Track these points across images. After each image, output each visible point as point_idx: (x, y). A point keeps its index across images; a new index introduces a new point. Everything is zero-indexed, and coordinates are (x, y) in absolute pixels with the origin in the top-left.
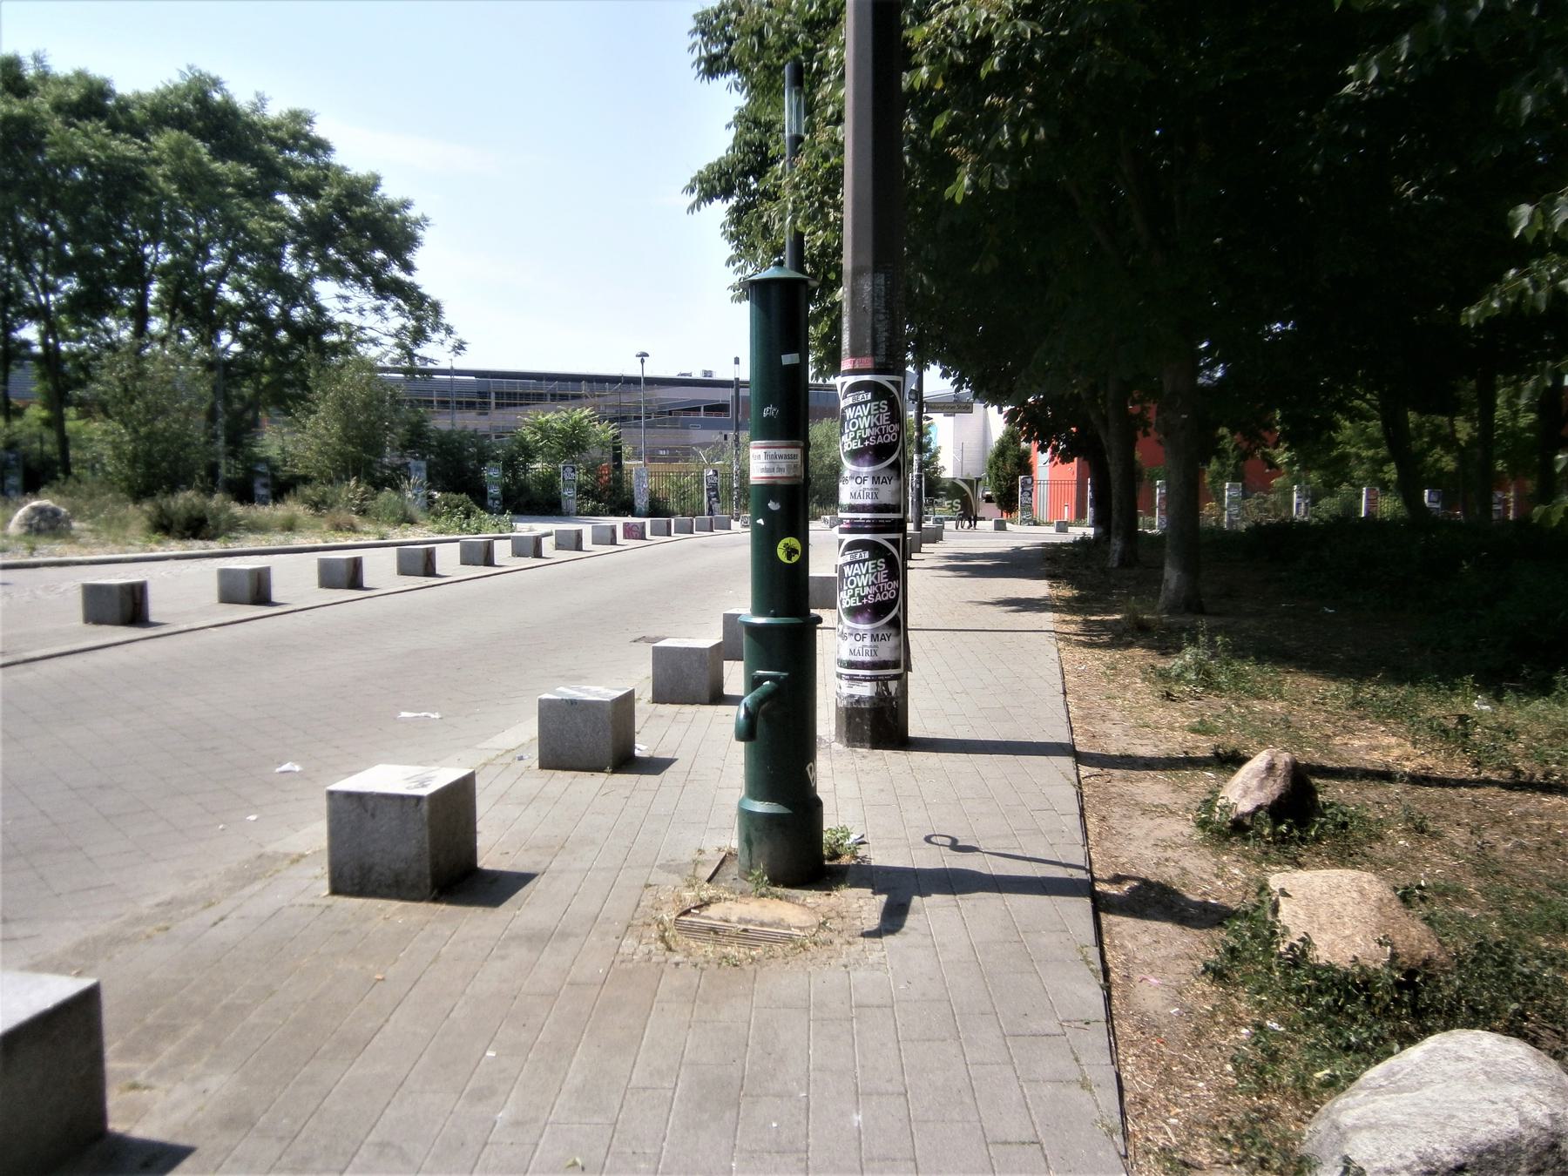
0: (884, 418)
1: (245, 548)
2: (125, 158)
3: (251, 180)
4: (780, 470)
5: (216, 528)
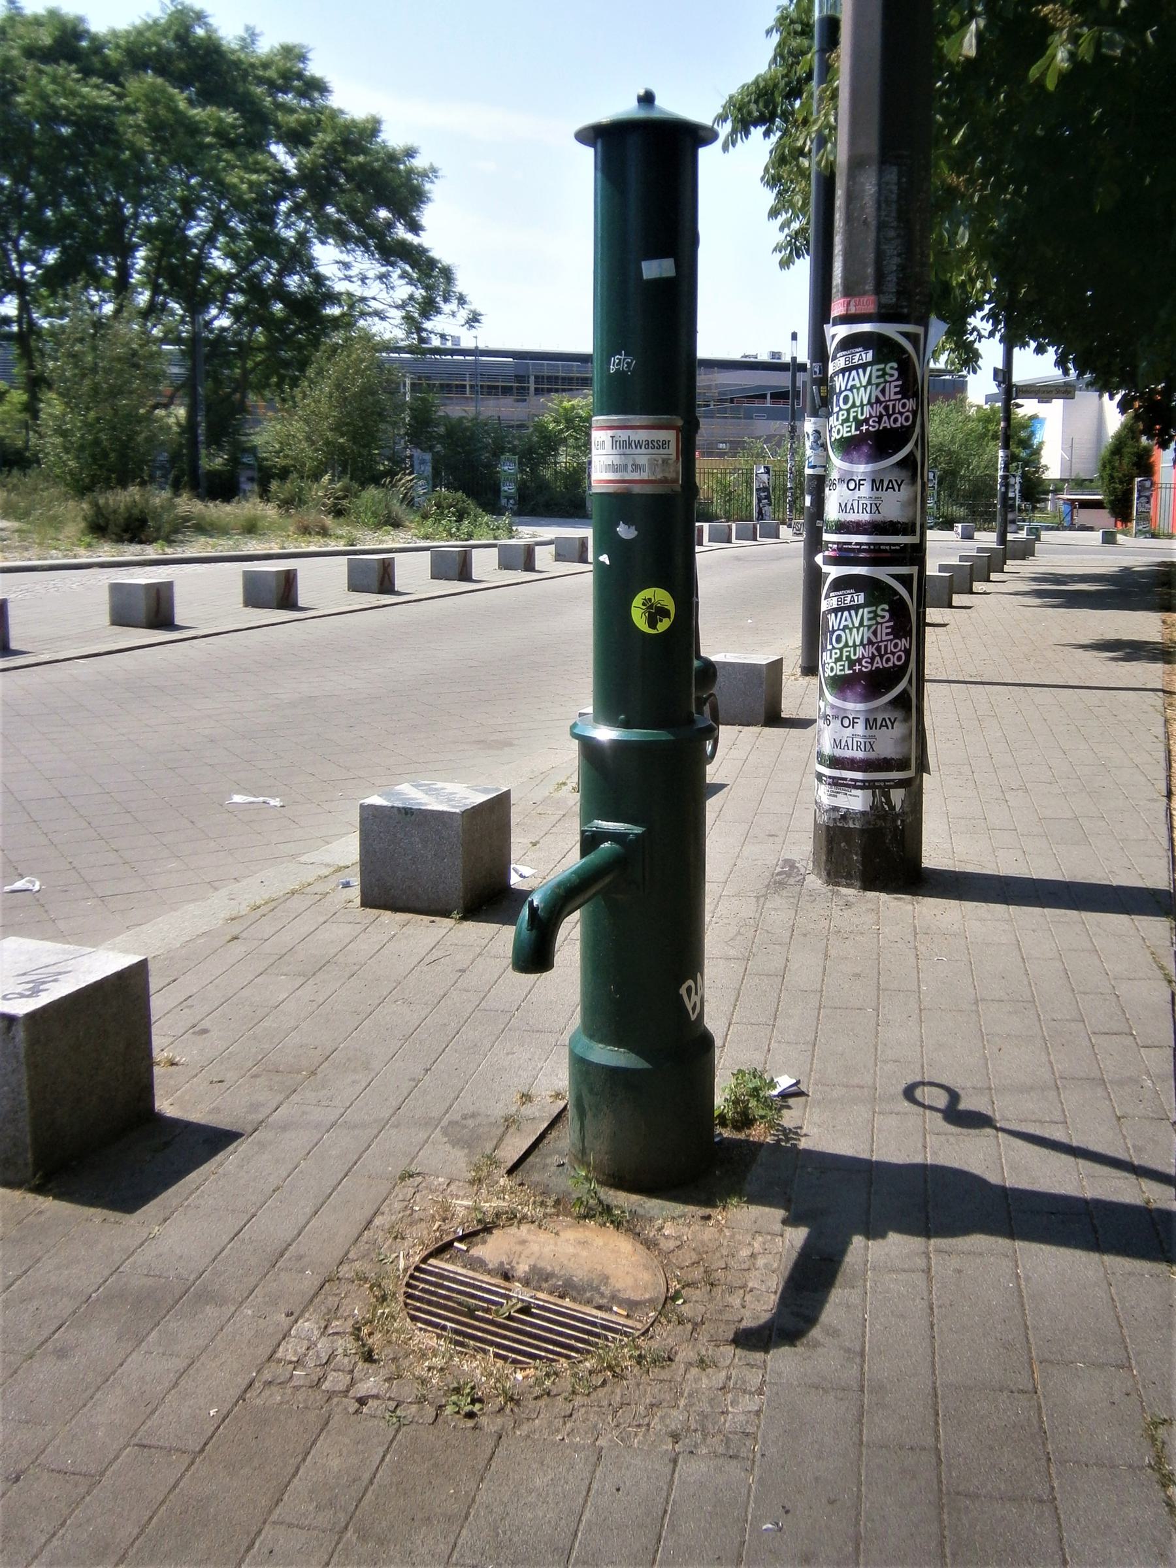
0: (892, 390)
1: (188, 555)
2: (97, 107)
3: (234, 127)
4: (637, 467)
5: (158, 529)
